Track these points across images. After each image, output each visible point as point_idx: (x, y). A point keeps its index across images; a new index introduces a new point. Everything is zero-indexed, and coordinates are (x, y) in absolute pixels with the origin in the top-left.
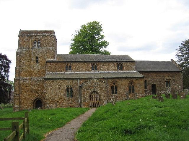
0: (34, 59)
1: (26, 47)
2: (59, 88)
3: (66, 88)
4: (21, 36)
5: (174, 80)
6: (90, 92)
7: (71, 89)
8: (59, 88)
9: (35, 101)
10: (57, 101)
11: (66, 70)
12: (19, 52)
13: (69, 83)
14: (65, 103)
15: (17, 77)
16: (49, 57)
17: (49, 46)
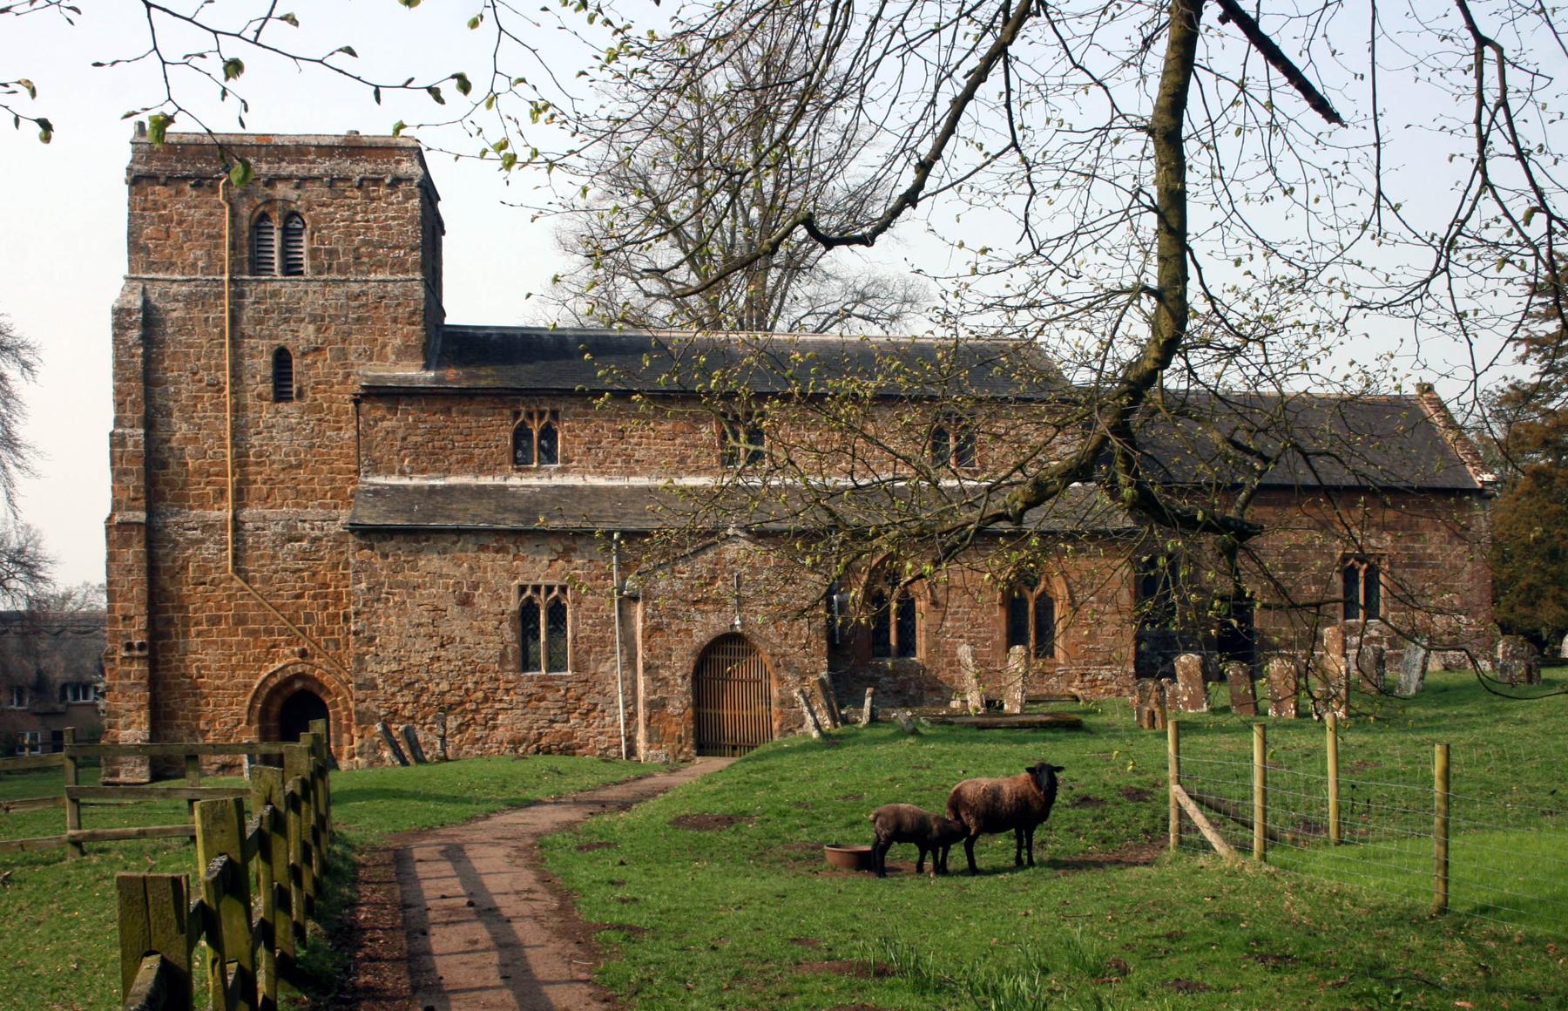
0: (261, 364)
1: (194, 265)
2: (465, 601)
3: (514, 605)
4: (152, 178)
5: (1416, 562)
6: (701, 636)
7: (557, 614)
8: (465, 601)
9: (278, 701)
10: (449, 698)
11: (520, 463)
12: (139, 303)
13: (540, 569)
14: (509, 724)
15: (129, 509)
16: (382, 357)
17: (380, 265)
